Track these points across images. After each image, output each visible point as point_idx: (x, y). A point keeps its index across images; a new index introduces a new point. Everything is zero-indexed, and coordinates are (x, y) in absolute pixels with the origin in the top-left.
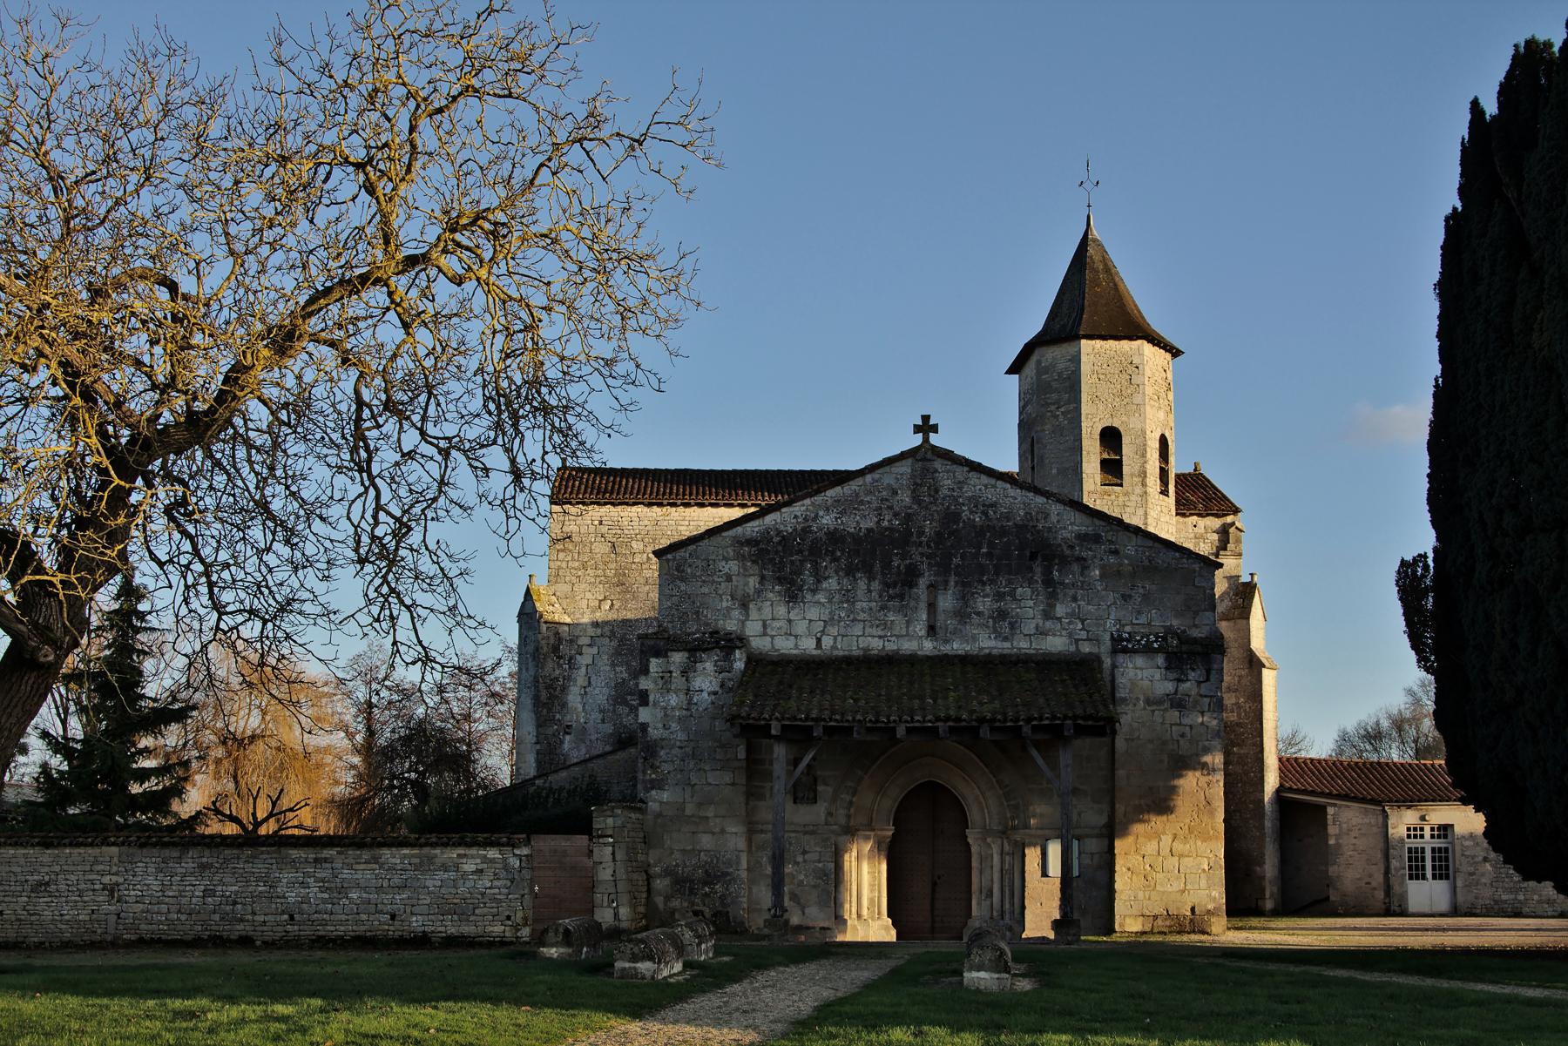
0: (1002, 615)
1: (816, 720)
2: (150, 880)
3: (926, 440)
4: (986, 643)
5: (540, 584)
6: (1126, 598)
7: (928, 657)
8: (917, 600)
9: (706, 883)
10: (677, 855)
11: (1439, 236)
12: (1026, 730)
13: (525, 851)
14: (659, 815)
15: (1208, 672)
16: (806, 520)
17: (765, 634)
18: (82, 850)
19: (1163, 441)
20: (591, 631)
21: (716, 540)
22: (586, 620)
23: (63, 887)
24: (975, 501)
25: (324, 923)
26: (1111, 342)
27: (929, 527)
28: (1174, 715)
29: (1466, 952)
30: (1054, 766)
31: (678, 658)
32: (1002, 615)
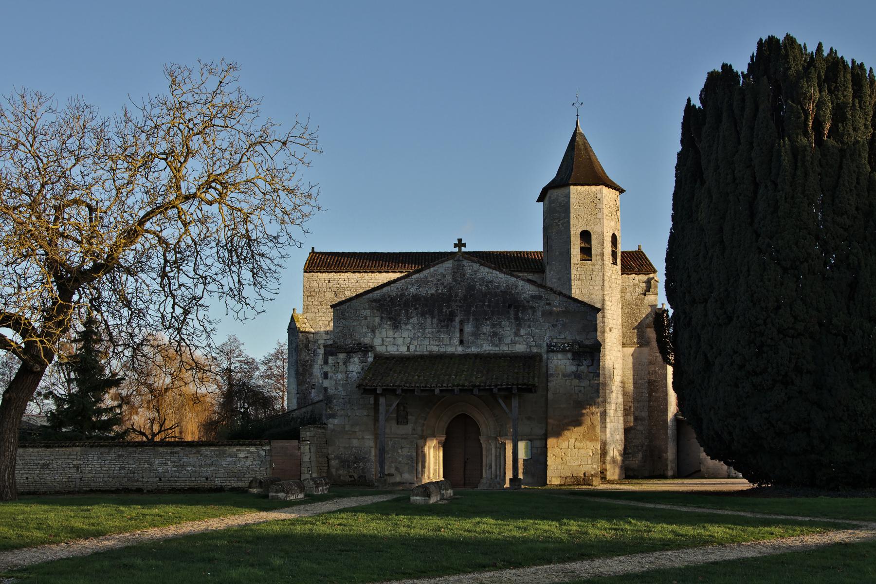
0: (495, 334)
1: (399, 386)
2: (95, 463)
3: (460, 250)
4: (487, 348)
5: (299, 311)
6: (554, 326)
7: (460, 355)
8: (455, 328)
9: (355, 463)
10: (341, 449)
11: (675, 161)
12: (495, 390)
13: (267, 448)
14: (333, 430)
15: (593, 361)
16: (402, 290)
17: (383, 345)
18: (64, 449)
19: (614, 237)
20: (324, 337)
21: (360, 300)
22: (322, 330)
23: (55, 466)
24: (482, 280)
25: (175, 482)
26: (586, 187)
27: (460, 293)
28: (576, 382)
29: (692, 493)
30: (509, 405)
31: (342, 356)
32: (495, 334)
